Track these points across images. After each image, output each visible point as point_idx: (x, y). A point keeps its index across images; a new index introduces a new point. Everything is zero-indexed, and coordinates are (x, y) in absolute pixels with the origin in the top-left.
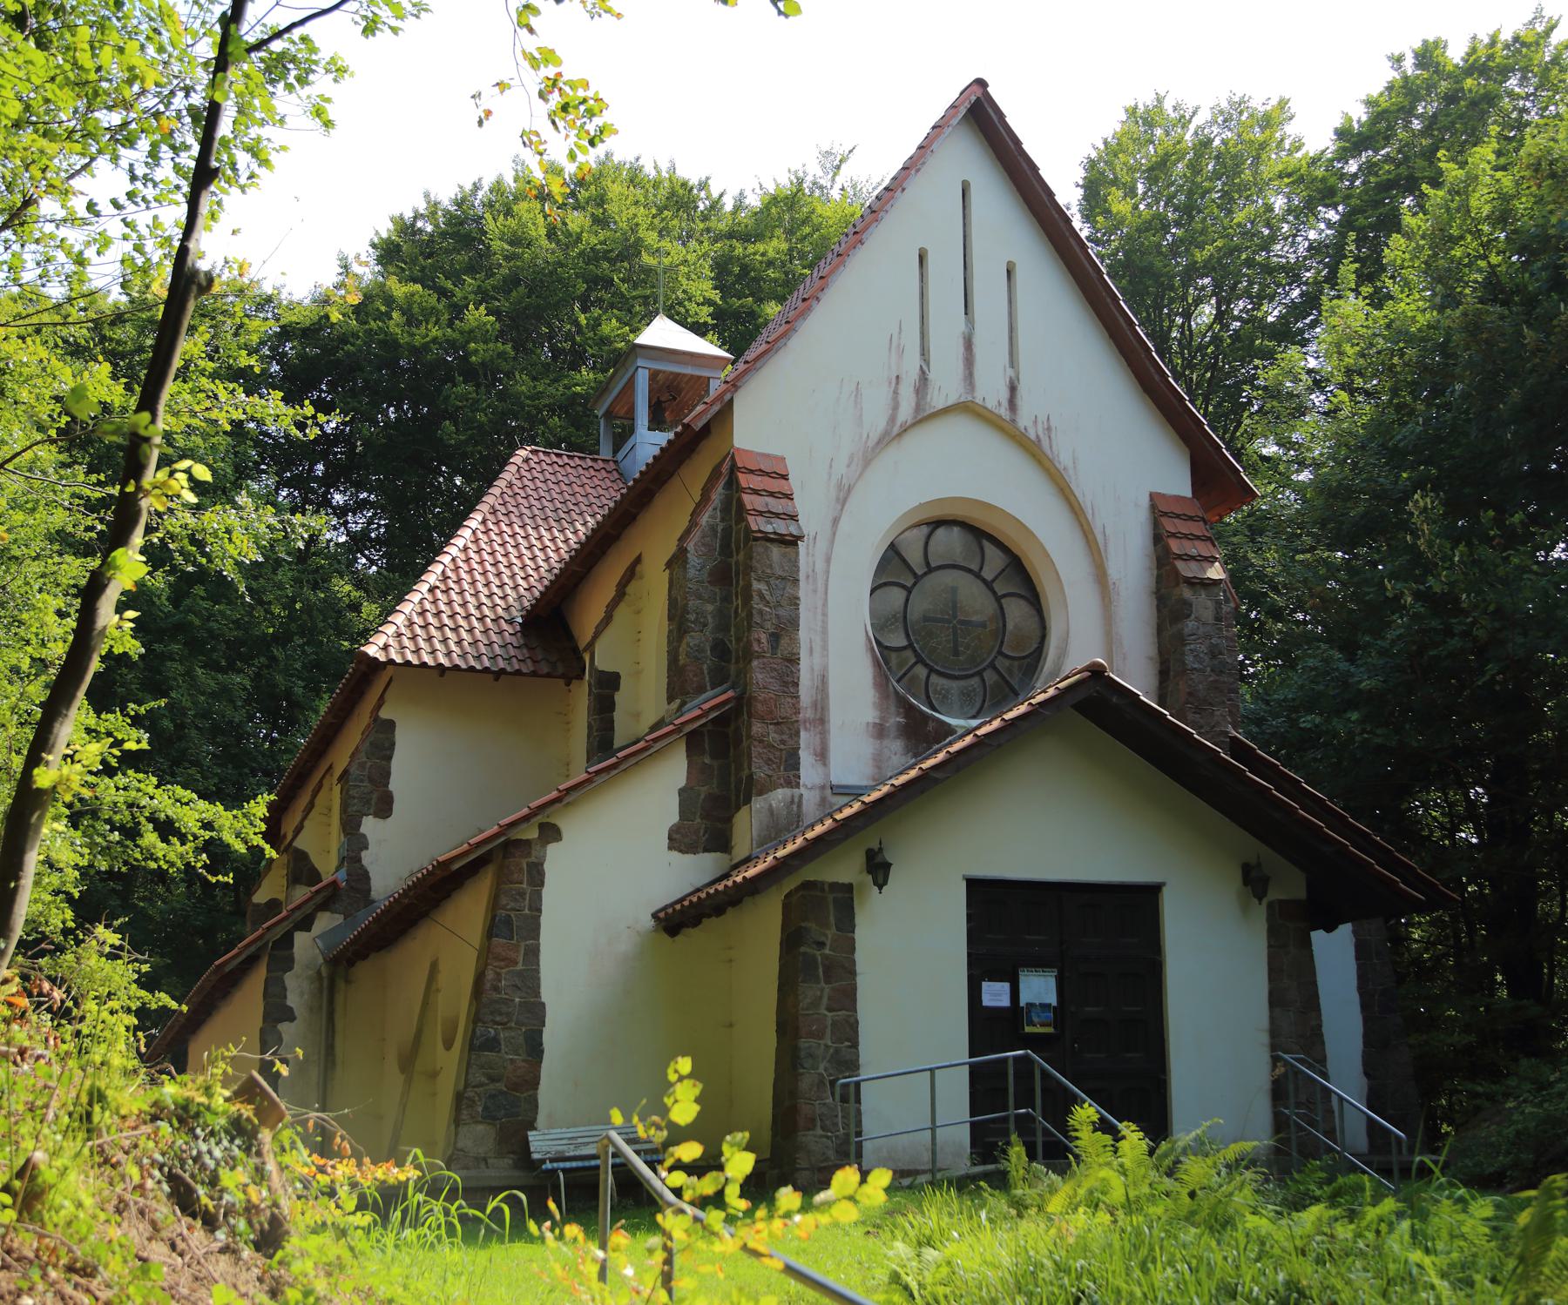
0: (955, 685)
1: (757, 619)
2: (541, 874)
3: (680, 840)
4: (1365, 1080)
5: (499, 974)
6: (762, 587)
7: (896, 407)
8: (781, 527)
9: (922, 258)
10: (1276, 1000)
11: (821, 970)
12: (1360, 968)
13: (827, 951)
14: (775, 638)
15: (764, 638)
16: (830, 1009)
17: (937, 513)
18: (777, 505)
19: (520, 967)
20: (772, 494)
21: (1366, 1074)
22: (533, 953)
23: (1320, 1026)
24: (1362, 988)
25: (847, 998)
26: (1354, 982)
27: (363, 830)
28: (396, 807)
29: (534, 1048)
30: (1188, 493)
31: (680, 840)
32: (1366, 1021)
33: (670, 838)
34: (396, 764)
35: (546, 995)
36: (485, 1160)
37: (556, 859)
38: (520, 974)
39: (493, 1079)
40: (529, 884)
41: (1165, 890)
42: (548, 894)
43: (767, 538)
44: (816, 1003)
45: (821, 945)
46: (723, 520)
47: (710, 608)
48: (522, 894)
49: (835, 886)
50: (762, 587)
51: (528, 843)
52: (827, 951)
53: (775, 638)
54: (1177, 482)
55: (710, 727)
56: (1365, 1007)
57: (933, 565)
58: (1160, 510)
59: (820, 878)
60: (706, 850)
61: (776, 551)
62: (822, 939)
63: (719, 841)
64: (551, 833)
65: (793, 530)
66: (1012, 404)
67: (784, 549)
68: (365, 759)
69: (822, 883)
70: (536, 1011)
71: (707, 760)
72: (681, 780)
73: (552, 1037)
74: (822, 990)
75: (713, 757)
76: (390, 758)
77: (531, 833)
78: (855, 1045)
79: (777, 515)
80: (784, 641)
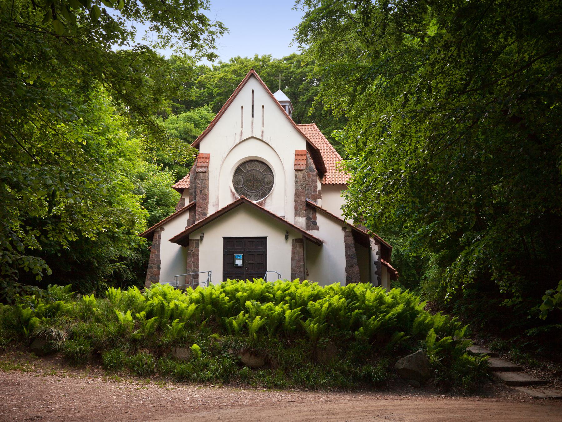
0: (253, 194)
1: (197, 188)
2: (160, 237)
7: (235, 140)
12: (346, 249)
14: (201, 191)
22: (159, 251)
24: (346, 254)
25: (197, 260)
26: (344, 253)
29: (159, 268)
32: (347, 261)
38: (157, 255)
41: (268, 239)
43: (199, 172)
44: (190, 261)
48: (157, 240)
49: (195, 240)
53: (201, 191)
56: (346, 258)
66: (262, 136)
70: (159, 262)
72: (188, 218)
73: (162, 266)
80: (203, 191)
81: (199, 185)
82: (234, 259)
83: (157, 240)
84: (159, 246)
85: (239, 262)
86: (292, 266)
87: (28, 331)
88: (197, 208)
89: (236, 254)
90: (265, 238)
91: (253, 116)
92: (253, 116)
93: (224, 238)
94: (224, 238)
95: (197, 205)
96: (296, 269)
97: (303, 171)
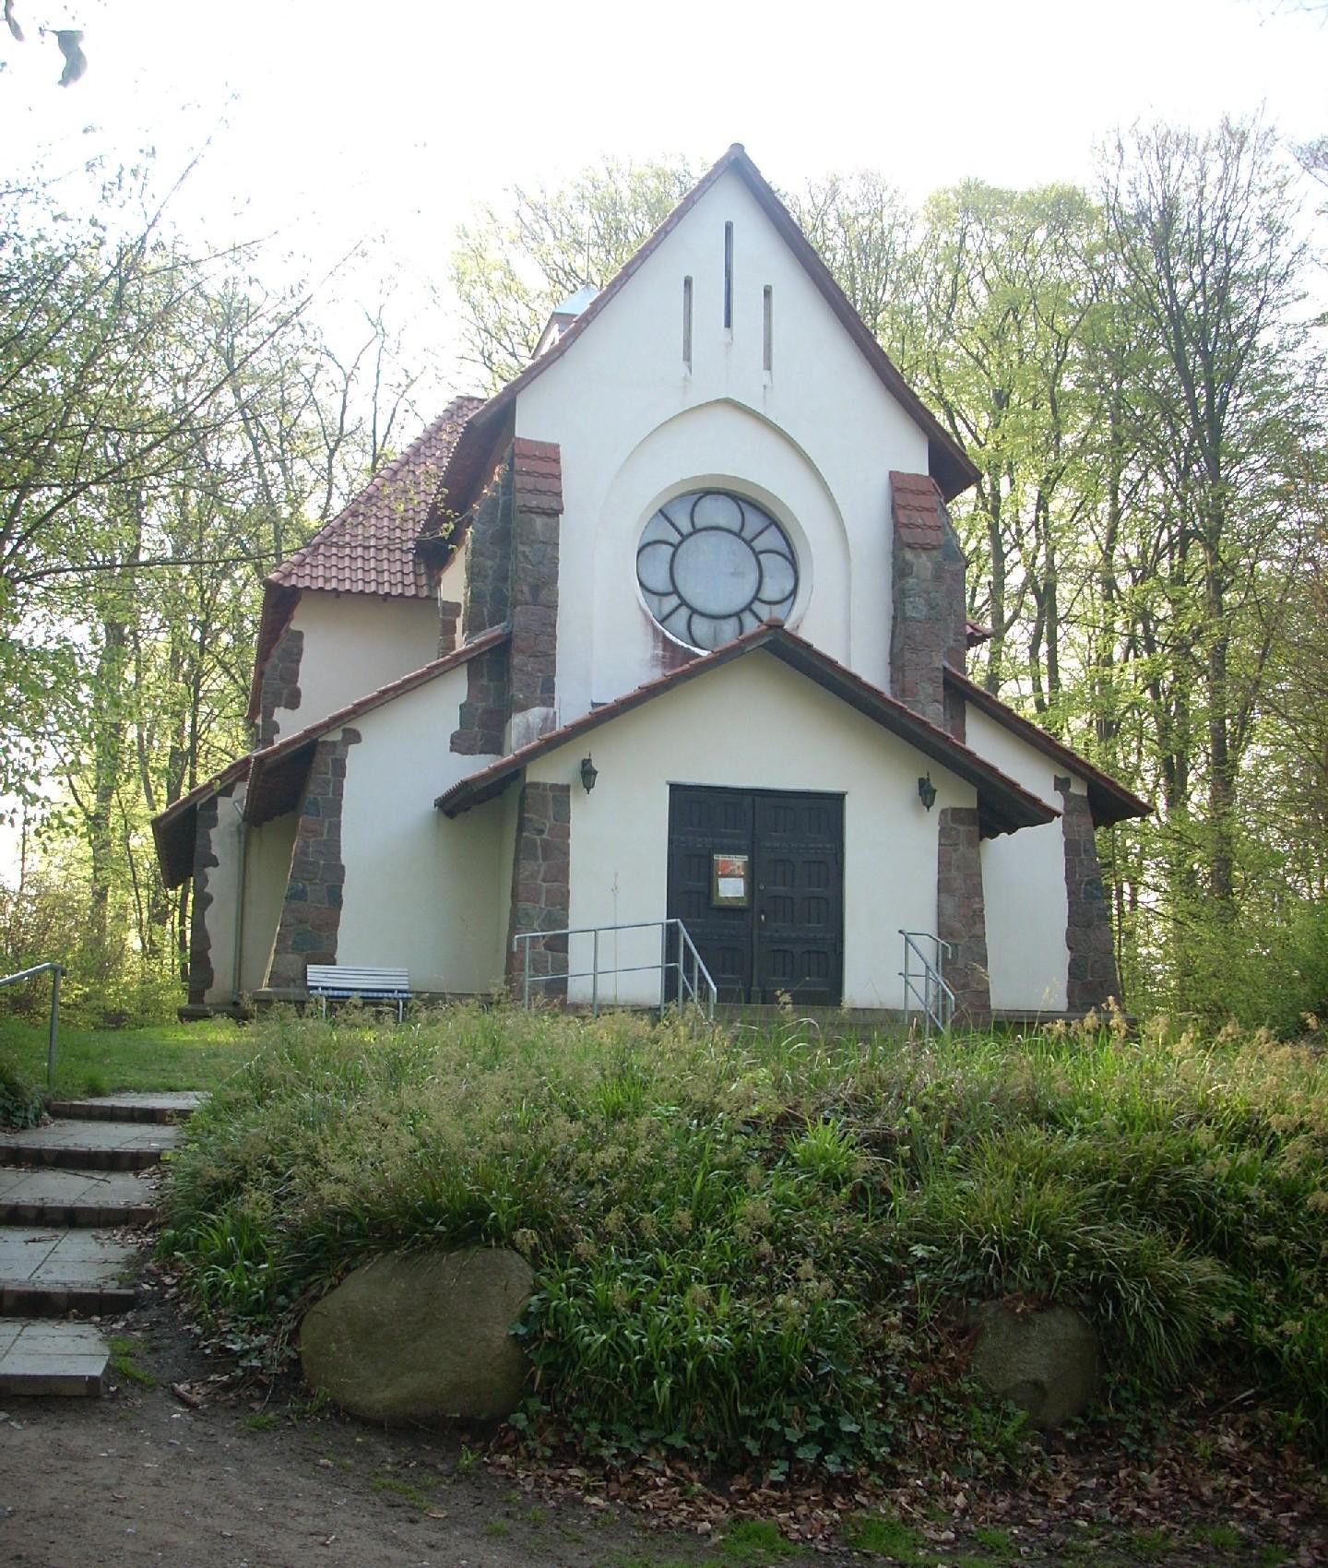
2: (343, 767)
3: (460, 744)
4: (1068, 952)
5: (307, 842)
6: (527, 549)
8: (546, 502)
9: (688, 283)
10: (943, 887)
11: (540, 851)
13: (545, 836)
14: (536, 589)
15: (526, 589)
16: (544, 881)
17: (708, 485)
18: (544, 484)
19: (325, 837)
20: (543, 475)
21: (1070, 948)
22: (336, 827)
23: (982, 910)
25: (561, 873)
27: (275, 718)
28: (303, 701)
29: (336, 900)
30: (927, 473)
31: (460, 744)
33: (452, 743)
34: (303, 668)
35: (345, 858)
36: (294, 980)
37: (355, 758)
39: (301, 922)
40: (334, 775)
41: (849, 804)
42: (347, 784)
43: (531, 510)
44: (533, 876)
45: (541, 832)
46: (504, 494)
47: (489, 563)
48: (327, 782)
49: (554, 787)
50: (527, 549)
51: (334, 744)
52: (545, 836)
53: (536, 589)
54: (916, 462)
55: (488, 656)
57: (698, 526)
58: (898, 484)
59: (540, 780)
60: (482, 752)
61: (539, 521)
62: (541, 827)
63: (496, 747)
64: (354, 737)
65: (554, 505)
67: (545, 519)
68: (276, 662)
69: (545, 784)
70: (339, 871)
71: (485, 682)
72: (463, 699)
74: (539, 866)
75: (490, 680)
76: (298, 661)
77: (336, 736)
78: (565, 908)
79: (544, 493)
81: (530, 562)
82: (709, 877)
83: (327, 782)
84: (336, 808)
85: (731, 888)
86: (940, 914)
87: (776, 1463)
88: (517, 660)
89: (719, 858)
90: (837, 799)
91: (728, 324)
92: (728, 324)
93: (675, 789)
94: (675, 789)
95: (517, 642)
96: (959, 925)
97: (935, 553)
